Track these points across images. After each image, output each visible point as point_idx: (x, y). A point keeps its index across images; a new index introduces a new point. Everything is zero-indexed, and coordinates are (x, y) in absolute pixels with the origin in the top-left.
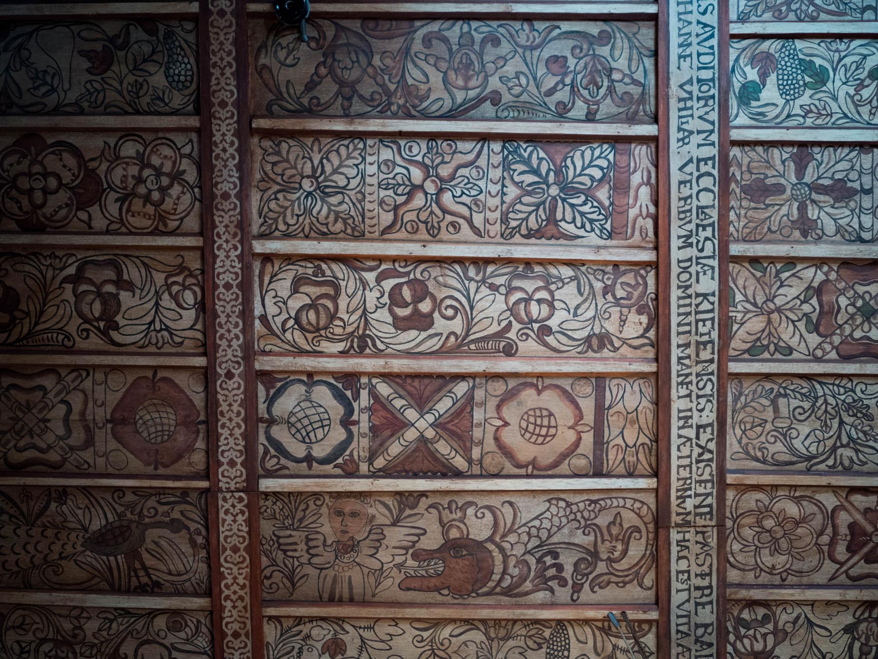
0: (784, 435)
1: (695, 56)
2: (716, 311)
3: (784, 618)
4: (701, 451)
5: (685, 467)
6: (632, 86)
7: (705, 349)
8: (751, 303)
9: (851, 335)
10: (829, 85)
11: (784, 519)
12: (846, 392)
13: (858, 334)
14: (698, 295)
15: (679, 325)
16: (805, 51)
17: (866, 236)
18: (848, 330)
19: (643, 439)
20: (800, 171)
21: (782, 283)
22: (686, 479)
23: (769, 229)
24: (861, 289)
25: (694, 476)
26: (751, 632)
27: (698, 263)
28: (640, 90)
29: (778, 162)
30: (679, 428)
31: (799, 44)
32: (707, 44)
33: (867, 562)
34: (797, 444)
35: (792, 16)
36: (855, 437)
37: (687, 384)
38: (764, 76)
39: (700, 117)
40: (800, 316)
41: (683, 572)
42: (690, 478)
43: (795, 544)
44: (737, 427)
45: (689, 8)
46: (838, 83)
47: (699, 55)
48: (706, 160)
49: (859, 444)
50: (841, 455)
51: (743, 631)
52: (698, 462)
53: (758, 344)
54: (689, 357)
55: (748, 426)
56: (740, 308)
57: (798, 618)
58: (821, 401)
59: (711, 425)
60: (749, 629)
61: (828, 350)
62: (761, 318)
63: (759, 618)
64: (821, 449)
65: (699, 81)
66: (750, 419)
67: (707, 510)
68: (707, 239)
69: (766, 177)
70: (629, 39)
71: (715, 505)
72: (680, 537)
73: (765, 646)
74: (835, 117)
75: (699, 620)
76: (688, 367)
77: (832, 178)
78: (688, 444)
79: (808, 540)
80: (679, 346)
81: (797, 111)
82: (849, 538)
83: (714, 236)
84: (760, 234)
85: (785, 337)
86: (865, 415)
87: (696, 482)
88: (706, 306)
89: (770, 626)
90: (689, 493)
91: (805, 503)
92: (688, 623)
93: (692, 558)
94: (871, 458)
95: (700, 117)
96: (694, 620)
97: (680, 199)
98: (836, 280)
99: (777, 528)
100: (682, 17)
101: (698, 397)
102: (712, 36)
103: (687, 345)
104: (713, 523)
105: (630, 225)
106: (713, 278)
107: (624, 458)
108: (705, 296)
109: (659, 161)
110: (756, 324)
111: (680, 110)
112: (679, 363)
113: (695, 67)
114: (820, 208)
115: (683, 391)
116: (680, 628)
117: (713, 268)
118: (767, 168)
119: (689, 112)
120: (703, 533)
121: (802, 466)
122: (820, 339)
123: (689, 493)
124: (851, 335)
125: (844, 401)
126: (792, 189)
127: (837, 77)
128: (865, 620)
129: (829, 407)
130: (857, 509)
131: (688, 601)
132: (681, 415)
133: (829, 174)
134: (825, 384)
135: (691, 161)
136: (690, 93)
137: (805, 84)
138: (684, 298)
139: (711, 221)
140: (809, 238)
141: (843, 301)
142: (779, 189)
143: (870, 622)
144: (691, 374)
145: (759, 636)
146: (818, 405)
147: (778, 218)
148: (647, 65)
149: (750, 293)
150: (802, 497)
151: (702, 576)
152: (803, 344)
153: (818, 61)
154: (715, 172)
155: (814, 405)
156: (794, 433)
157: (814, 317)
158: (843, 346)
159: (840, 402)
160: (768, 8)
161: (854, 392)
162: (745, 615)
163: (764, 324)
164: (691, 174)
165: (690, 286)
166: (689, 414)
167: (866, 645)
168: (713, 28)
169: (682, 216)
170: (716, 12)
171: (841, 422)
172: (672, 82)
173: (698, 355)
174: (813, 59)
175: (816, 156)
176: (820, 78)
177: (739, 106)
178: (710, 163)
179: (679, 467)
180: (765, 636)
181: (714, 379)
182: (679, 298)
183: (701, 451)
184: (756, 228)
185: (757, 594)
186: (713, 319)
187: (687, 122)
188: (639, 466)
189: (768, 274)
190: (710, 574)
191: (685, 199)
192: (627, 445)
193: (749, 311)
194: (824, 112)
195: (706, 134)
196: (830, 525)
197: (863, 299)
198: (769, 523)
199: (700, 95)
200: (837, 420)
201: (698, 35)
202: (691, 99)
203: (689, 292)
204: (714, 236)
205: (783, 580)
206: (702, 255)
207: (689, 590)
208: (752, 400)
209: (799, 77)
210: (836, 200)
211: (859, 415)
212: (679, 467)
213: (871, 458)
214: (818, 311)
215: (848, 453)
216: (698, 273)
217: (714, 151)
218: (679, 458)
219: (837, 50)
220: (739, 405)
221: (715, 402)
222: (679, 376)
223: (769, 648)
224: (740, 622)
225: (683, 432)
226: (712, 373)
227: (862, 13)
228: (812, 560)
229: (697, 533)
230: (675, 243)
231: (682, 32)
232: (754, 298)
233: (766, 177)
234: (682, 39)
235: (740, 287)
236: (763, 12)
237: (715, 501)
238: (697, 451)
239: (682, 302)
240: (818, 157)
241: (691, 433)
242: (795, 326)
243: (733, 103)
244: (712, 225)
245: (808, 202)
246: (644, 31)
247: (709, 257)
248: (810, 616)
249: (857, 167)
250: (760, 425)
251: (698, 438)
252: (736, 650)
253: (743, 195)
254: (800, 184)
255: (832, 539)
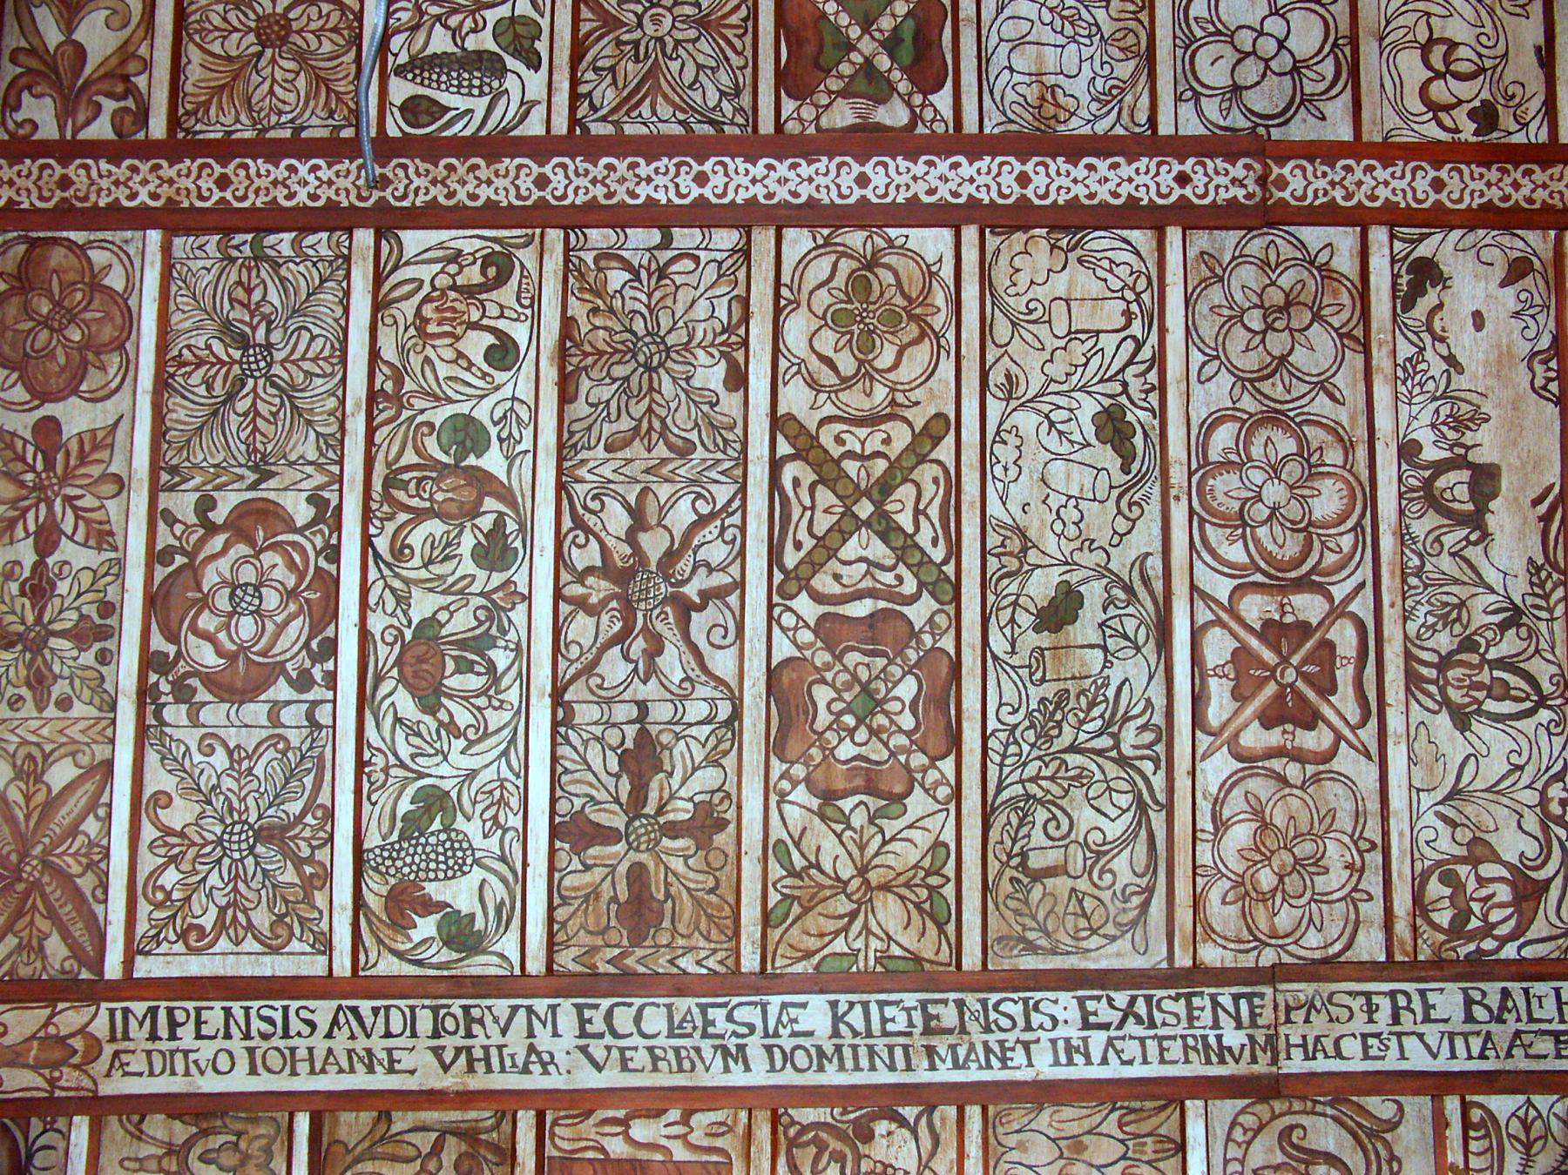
0: (1099, 855)
1: (391, 1043)
2: (865, 997)
3: (1445, 844)
4: (1131, 1020)
5: (1162, 1050)
6: (444, 1156)
7: (937, 1017)
8: (850, 923)
9: (908, 734)
10: (446, 785)
11: (1258, 850)
12: (1016, 742)
13: (907, 721)
14: (836, 1033)
15: (892, 1067)
16: (385, 830)
17: (724, 710)
18: (900, 740)
19: (1110, 1126)
20: (607, 835)
21: (811, 866)
22: (1186, 1046)
23: (712, 891)
24: (824, 718)
25: (1179, 1031)
26: (1476, 907)
27: (776, 1035)
28: (451, 1141)
29: (587, 878)
30: (1089, 1062)
31: (373, 840)
32: (369, 1021)
33: (1333, 691)
34: (1114, 830)
35: (322, 855)
36: (1099, 722)
37: (1004, 1049)
38: (428, 906)
39: (504, 1032)
40: (874, 829)
41: (1366, 1047)
42: (1183, 1037)
43: (1304, 828)
44: (1084, 944)
45: (302, 1053)
46: (445, 769)
47: (388, 1034)
48: (583, 1022)
49: (1113, 714)
50: (1135, 747)
51: (1474, 923)
52: (1152, 1025)
53: (927, 906)
54: (953, 1048)
55: (1083, 923)
56: (859, 944)
57: (1444, 818)
58: (1033, 789)
59: (1081, 1002)
60: (1471, 911)
61: (937, 775)
62: (878, 904)
63: (1447, 891)
64: (1125, 786)
65: (436, 1035)
66: (1070, 919)
67: (1243, 1004)
68: (730, 1018)
69: (614, 899)
70: (357, 1161)
71: (1235, 990)
72: (1297, 1054)
73: (1502, 879)
74: (506, 773)
75: (1458, 1014)
76: (972, 1048)
77: (617, 776)
78: (1118, 1044)
79: (1295, 803)
80: (933, 1068)
81: (493, 844)
82: (1289, 727)
83: (725, 1005)
84: (721, 910)
85: (913, 856)
86: (1058, 706)
87: (1191, 1026)
88: (856, 1018)
89: (1463, 870)
90: (1212, 1040)
91: (1226, 813)
92: (1465, 1035)
93: (1339, 1029)
94: (1138, 692)
95: (504, 1032)
96: (1457, 1023)
97: (655, 1069)
98: (807, 765)
99: (1276, 862)
100: (318, 1066)
101: (1028, 1027)
102: (354, 1010)
103: (931, 1051)
104: (1268, 991)
105: (705, 1158)
106: (804, 1005)
107: (1149, 1163)
108: (837, 1019)
109: (581, 1102)
110: (889, 912)
111: (489, 1070)
112: (964, 1067)
113: (410, 1043)
114: (672, 797)
115: (1019, 1057)
116: (1475, 1051)
117: (784, 1006)
118: (597, 898)
119: (494, 1052)
120: (1288, 1009)
121: (1158, 820)
122: (917, 789)
123: (1212, 1040)
124: (908, 734)
125: (1033, 746)
126: (637, 850)
127: (432, 771)
128: (1442, 691)
129: (1045, 773)
130: (1236, 713)
131: (1421, 1036)
132: (1063, 1059)
133: (610, 782)
134: (1000, 782)
135: (584, 1050)
136: (458, 1050)
137: (447, 829)
138: (841, 1059)
139: (695, 1010)
140: (728, 816)
141: (846, 751)
142: (637, 874)
143: (1447, 683)
144: (985, 1044)
145: (1484, 892)
146: (1040, 794)
147: (692, 875)
148: (406, 1126)
149: (832, 926)
150: (1215, 818)
151: (1371, 1010)
152: (926, 823)
153: (405, 806)
154: (606, 1003)
155: (1041, 802)
156: (1096, 837)
157: (874, 803)
158: (930, 747)
159: (1036, 753)
160: (308, 900)
161: (1016, 726)
162: (1443, 918)
163: (890, 897)
164: (608, 1048)
165: (819, 1048)
166: (1061, 1044)
167: (1489, 689)
168: (340, 1008)
169: (687, 1065)
170: (311, 1004)
171: (1073, 748)
172: (438, 1085)
173: (950, 1031)
174: (400, 814)
175: (577, 807)
176: (435, 802)
177: (484, 952)
178: (587, 1014)
179: (1162, 1061)
180: (1482, 881)
181: (994, 998)
182: (842, 1068)
183: (1131, 1020)
184: (709, 917)
185: (1402, 902)
186: (882, 1004)
187: (512, 1056)
188: (1162, 1131)
189: (797, 893)
190: (1368, 995)
191: (655, 1059)
192: (1124, 1157)
193: (866, 925)
194: (497, 793)
195: (535, 1021)
196: (1267, 764)
197: (840, 714)
198: (1266, 879)
199: (462, 1032)
200: (1066, 756)
201: (353, 1037)
202: (469, 1049)
203: (829, 1048)
204: (725, 1005)
205: (1374, 845)
206: (759, 1023)
207: (1399, 1035)
208: (1034, 918)
209: (433, 840)
210: (658, 768)
211: (1058, 717)
212: (1162, 1061)
213: (1138, 692)
214: (864, 798)
215: (1129, 736)
216: (794, 1034)
217: (566, 1006)
218: (1145, 1061)
219: (386, 770)
220: (1043, 942)
221: (1038, 995)
222: (989, 1066)
223: (1505, 873)
224: (1457, 930)
225: (1096, 1056)
226: (984, 1003)
227: (320, 727)
228: (1334, 793)
229: (1288, 1021)
230: (738, 1078)
231: (345, 1065)
232: (841, 917)
233: (614, 899)
234: (359, 1066)
235: (819, 944)
236: (314, 907)
237: (1226, 990)
238: (1131, 1027)
239: (849, 1064)
240: (578, 802)
241: (1098, 1039)
242: (893, 839)
243: (480, 965)
244: (703, 1009)
245: (662, 820)
246: (342, 1133)
247: (764, 1013)
248: (1439, 795)
249: (597, 730)
250: (1080, 902)
251: (1106, 1026)
252: (1512, 937)
253: (649, 942)
254: (627, 836)
255: (1294, 758)
